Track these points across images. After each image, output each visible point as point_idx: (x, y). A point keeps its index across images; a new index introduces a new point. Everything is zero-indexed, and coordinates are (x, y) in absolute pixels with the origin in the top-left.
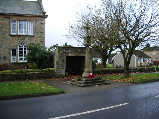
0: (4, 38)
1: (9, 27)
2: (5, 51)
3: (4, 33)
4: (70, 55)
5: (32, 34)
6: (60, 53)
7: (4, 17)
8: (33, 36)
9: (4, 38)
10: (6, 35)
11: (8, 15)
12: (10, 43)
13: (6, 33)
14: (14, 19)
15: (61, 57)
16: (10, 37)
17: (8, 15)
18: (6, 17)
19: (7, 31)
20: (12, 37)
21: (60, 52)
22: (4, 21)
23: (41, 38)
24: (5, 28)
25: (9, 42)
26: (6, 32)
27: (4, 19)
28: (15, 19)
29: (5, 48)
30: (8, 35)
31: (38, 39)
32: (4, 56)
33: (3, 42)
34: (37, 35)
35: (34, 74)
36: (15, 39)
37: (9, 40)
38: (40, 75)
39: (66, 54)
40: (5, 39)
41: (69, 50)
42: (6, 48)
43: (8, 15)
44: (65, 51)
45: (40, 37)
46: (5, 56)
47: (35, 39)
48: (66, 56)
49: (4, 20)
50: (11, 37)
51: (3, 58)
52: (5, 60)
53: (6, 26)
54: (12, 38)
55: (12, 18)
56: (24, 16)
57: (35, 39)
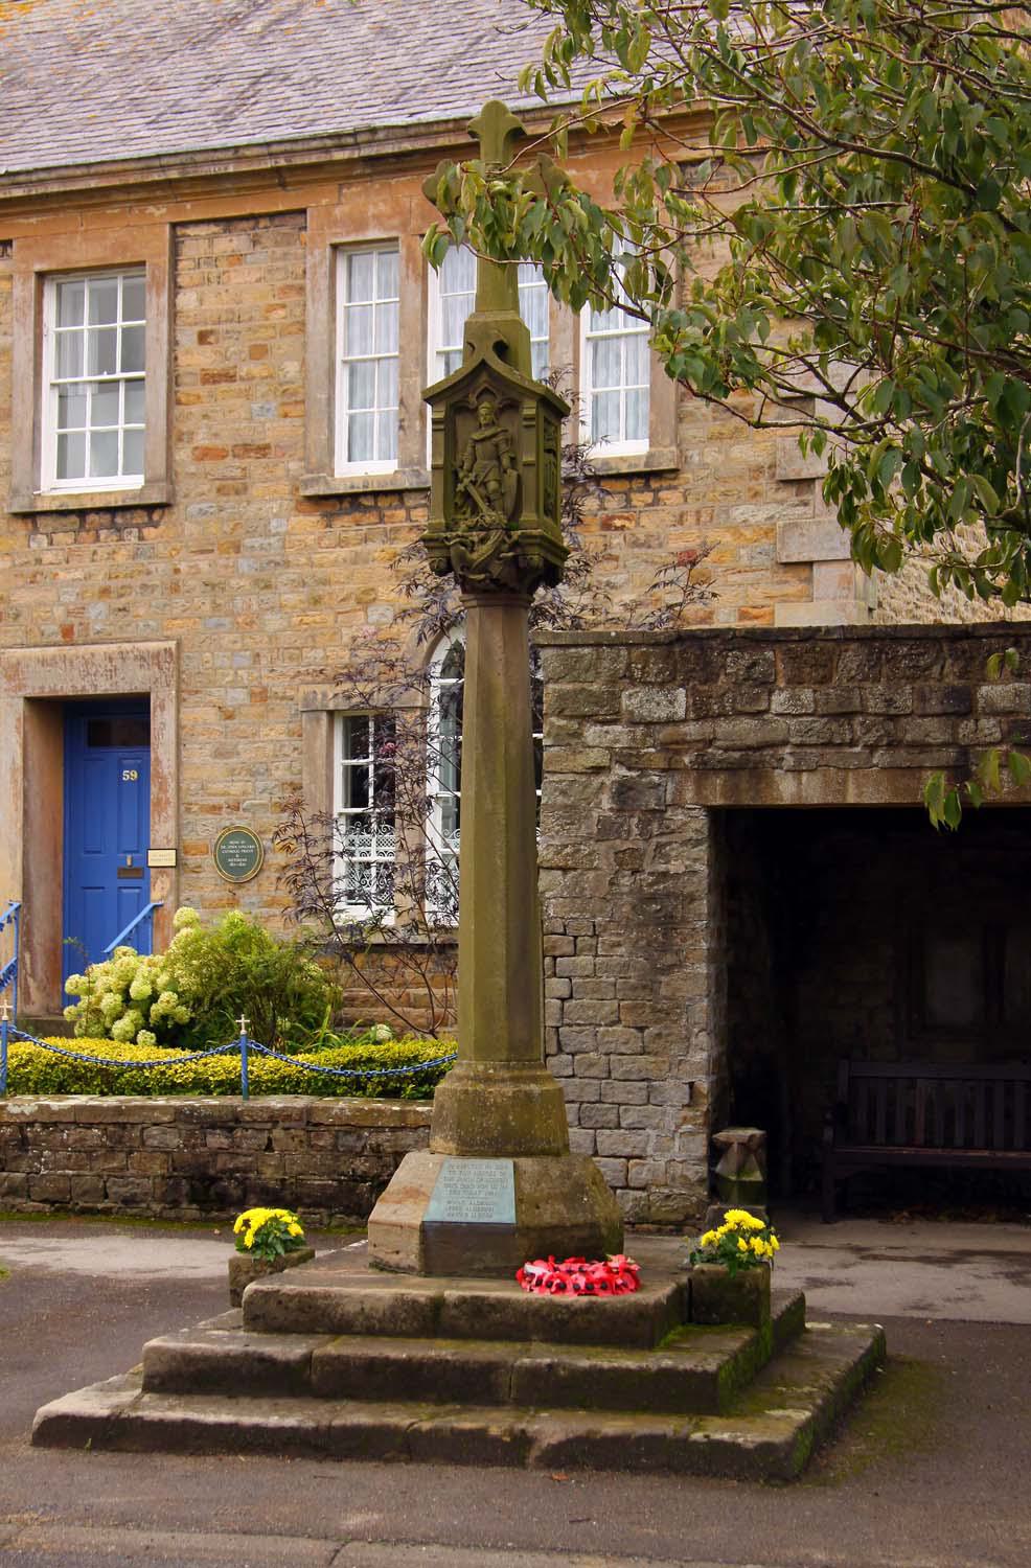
0: (237, 548)
1: (292, 368)
2: (247, 753)
3: (231, 467)
4: (788, 789)
5: (126, 484)
6: (595, 757)
7: (228, 222)
8: (648, 477)
9: (237, 548)
10: (256, 491)
11: (277, 170)
12: (314, 616)
13: (254, 464)
14: (361, 225)
15: (606, 830)
16: (309, 524)
17: (280, 178)
18: (254, 217)
19: (274, 429)
20: (345, 525)
21: (592, 733)
22: (240, 277)
23: (788, 494)
24: (247, 395)
25: (291, 598)
26: (263, 450)
27: (236, 242)
28: (379, 220)
29: (241, 696)
30: (285, 488)
31: (740, 513)
32: (228, 819)
33: (216, 606)
34: (712, 455)
35: (119, 1127)
36: (375, 548)
37: (291, 574)
38: (217, 1140)
39: (704, 769)
40: (244, 564)
41: (779, 701)
42: (261, 696)
43: (280, 178)
44: (701, 712)
45: (764, 484)
46: (240, 821)
47: (681, 519)
48: (713, 813)
49: (237, 258)
50: (329, 518)
51: (223, 861)
52: (249, 895)
53: (259, 352)
54: (342, 543)
55: (263, 223)
56: (47, 196)
57: (681, 519)
